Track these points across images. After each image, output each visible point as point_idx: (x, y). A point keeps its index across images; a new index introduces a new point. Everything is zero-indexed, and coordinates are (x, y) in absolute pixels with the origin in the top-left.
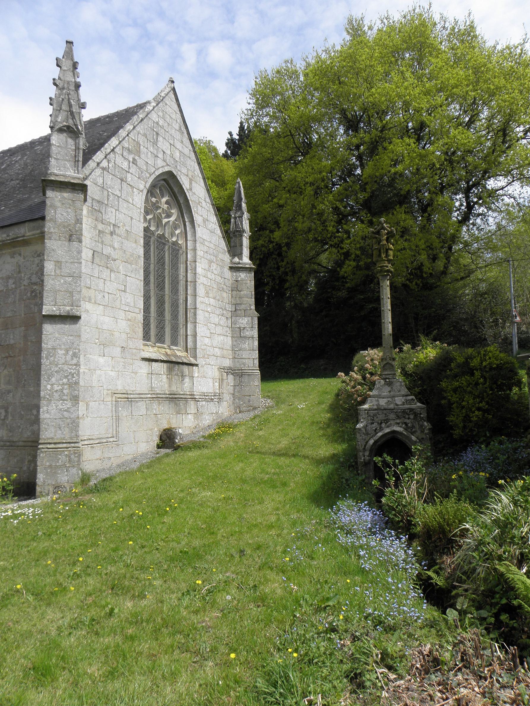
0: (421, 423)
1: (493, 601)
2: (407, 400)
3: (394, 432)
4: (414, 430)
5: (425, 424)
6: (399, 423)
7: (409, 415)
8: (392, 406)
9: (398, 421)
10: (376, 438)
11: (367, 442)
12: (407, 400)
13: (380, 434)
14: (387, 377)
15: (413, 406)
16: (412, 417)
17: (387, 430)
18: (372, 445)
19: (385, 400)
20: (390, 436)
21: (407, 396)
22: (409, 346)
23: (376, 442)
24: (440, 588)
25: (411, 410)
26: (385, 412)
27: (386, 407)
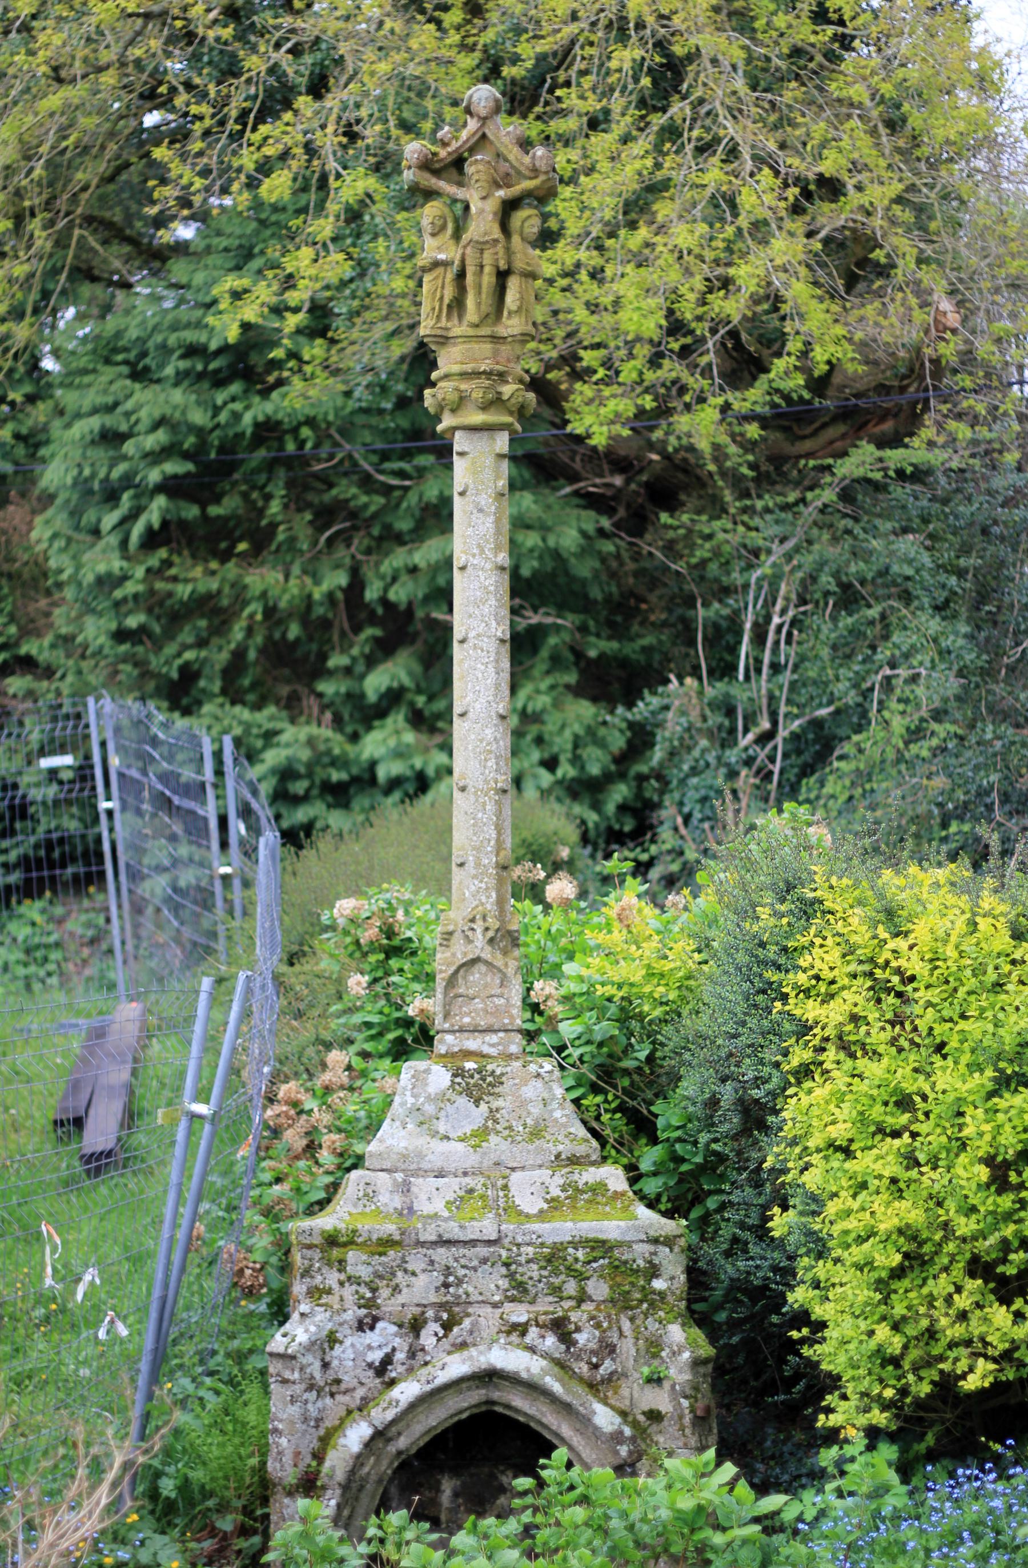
0: (652, 1325)
1: (214, 511)
2: (574, 1191)
3: (490, 1376)
4: (608, 1366)
5: (676, 1333)
6: (521, 1329)
7: (581, 1278)
8: (486, 1227)
9: (519, 1314)
10: (381, 1415)
11: (325, 1441)
12: (574, 1191)
13: (407, 1391)
14: (472, 1044)
15: (612, 1228)
16: (599, 1289)
17: (457, 1367)
18: (359, 1460)
19: (452, 1187)
20: (471, 1399)
21: (574, 1161)
22: (972, 1383)
23: (381, 1435)
24: (442, 1472)
25: (601, 1247)
26: (441, 1255)
27: (452, 1230)
